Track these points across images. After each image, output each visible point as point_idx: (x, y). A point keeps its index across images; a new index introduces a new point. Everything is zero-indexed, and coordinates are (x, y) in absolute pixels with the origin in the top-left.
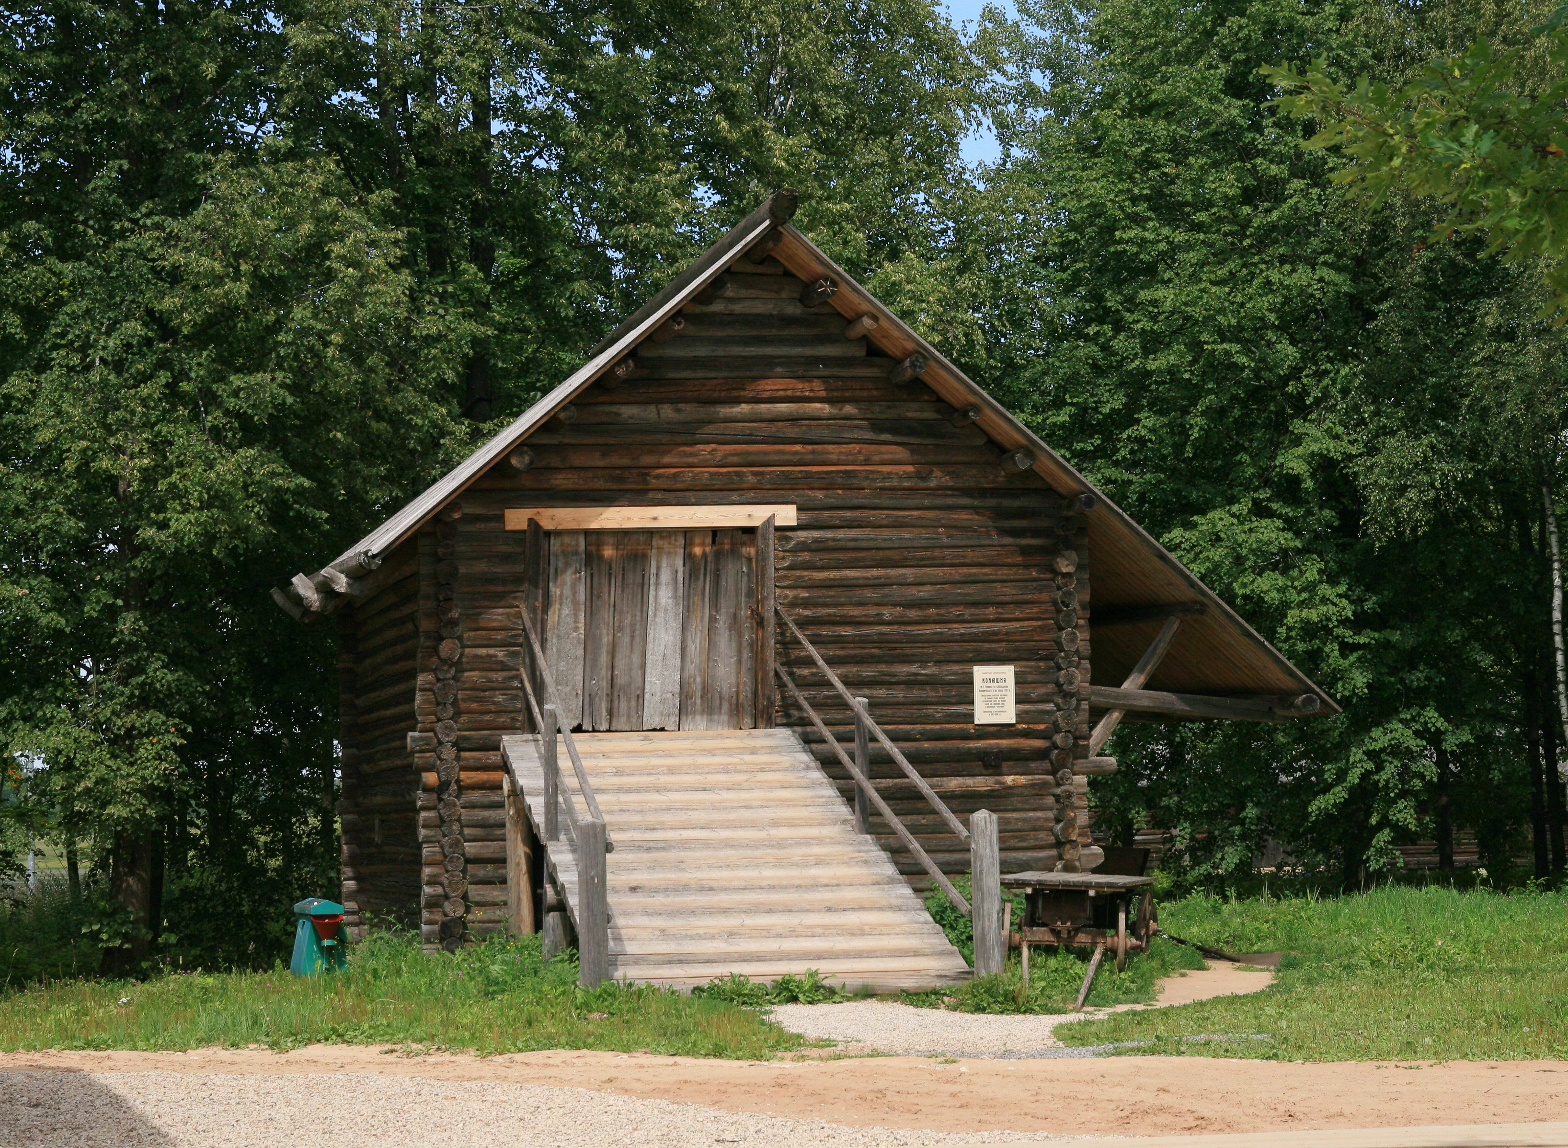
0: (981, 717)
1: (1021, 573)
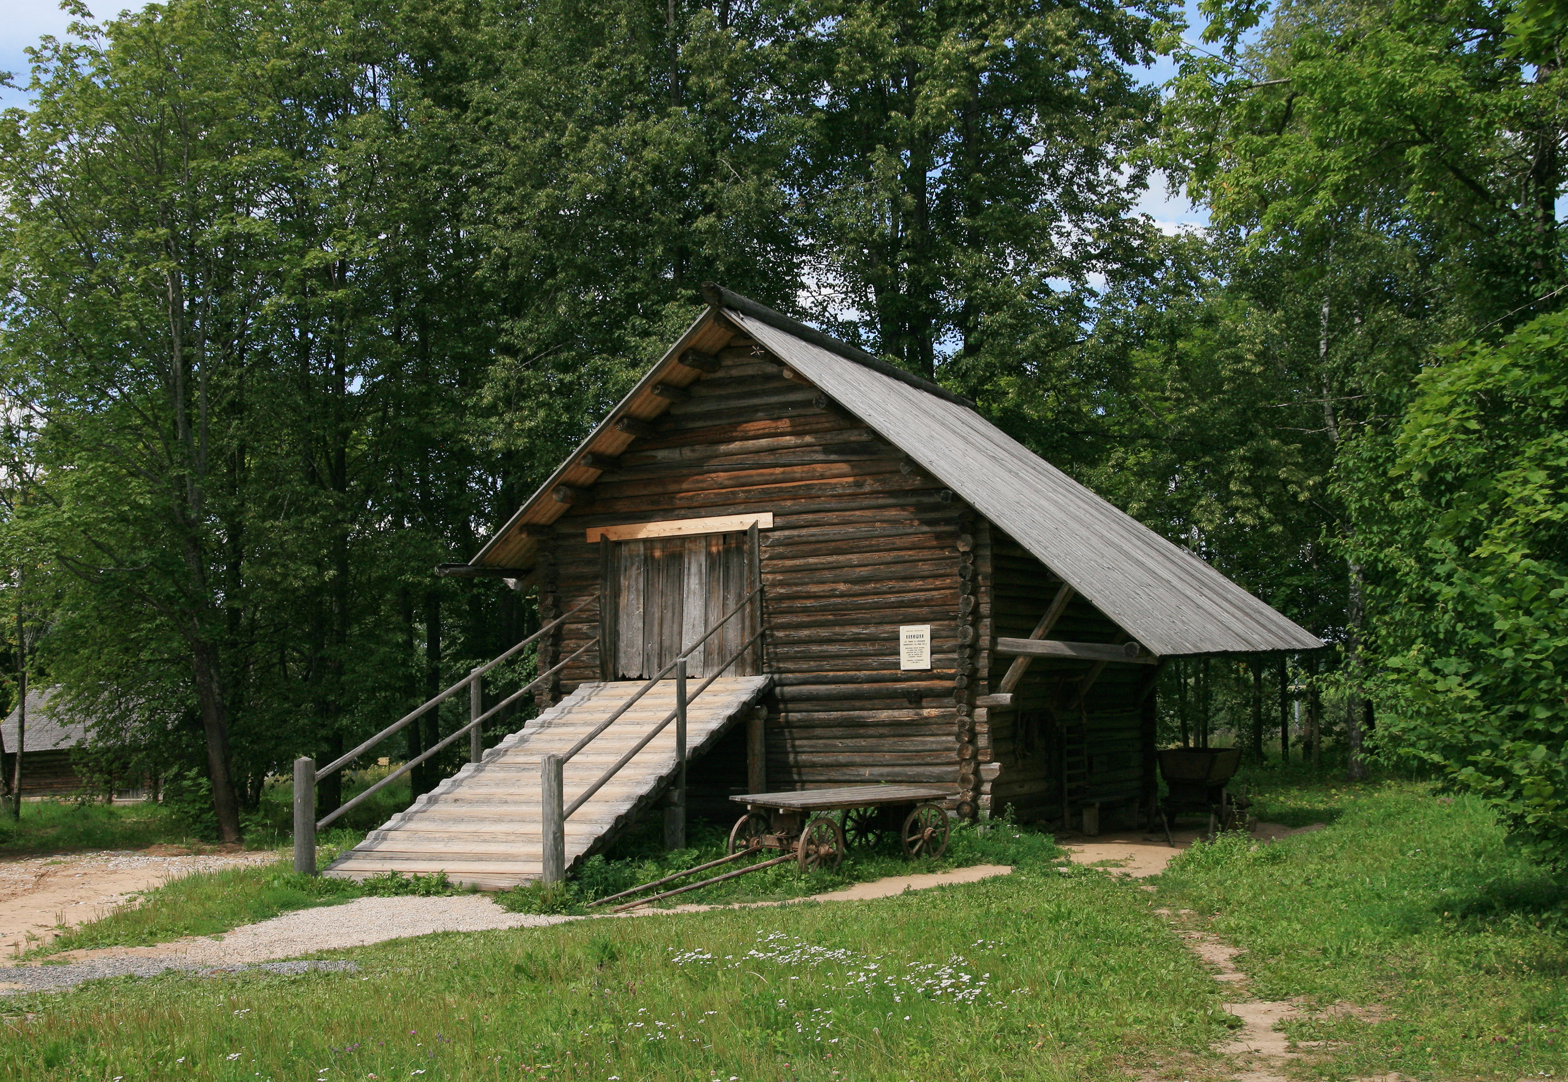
1: (938, 553)
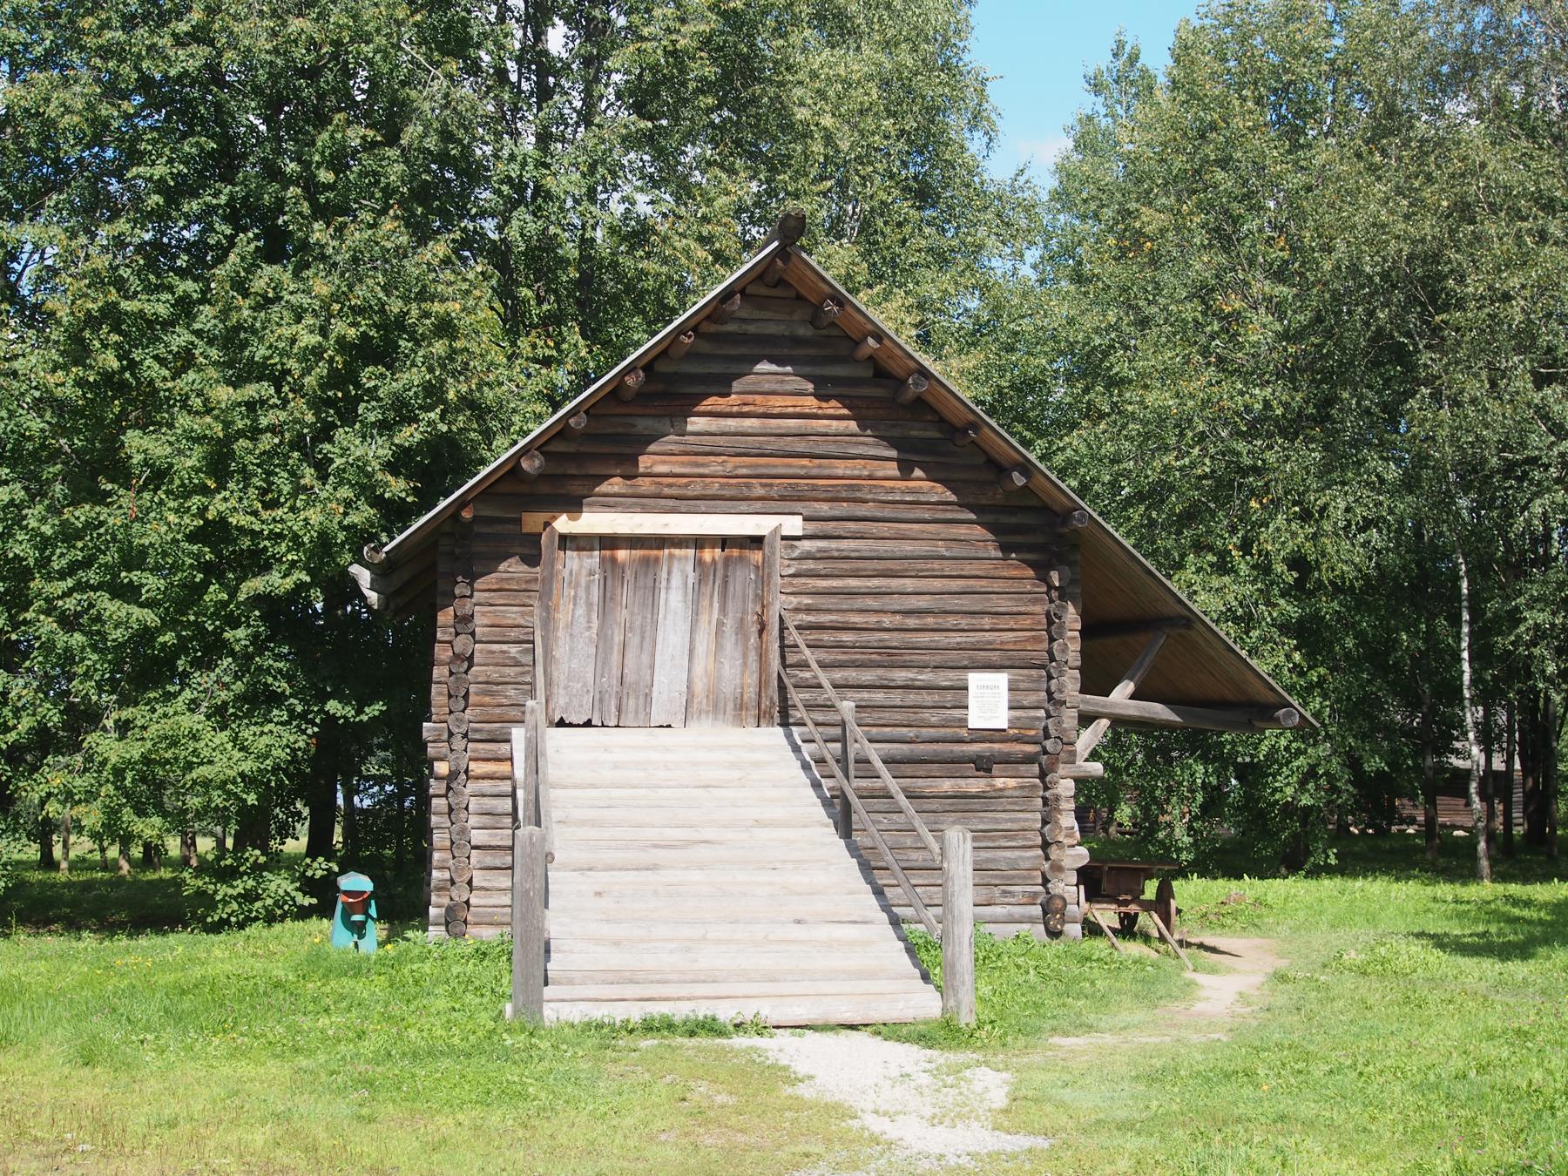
0: (973, 723)
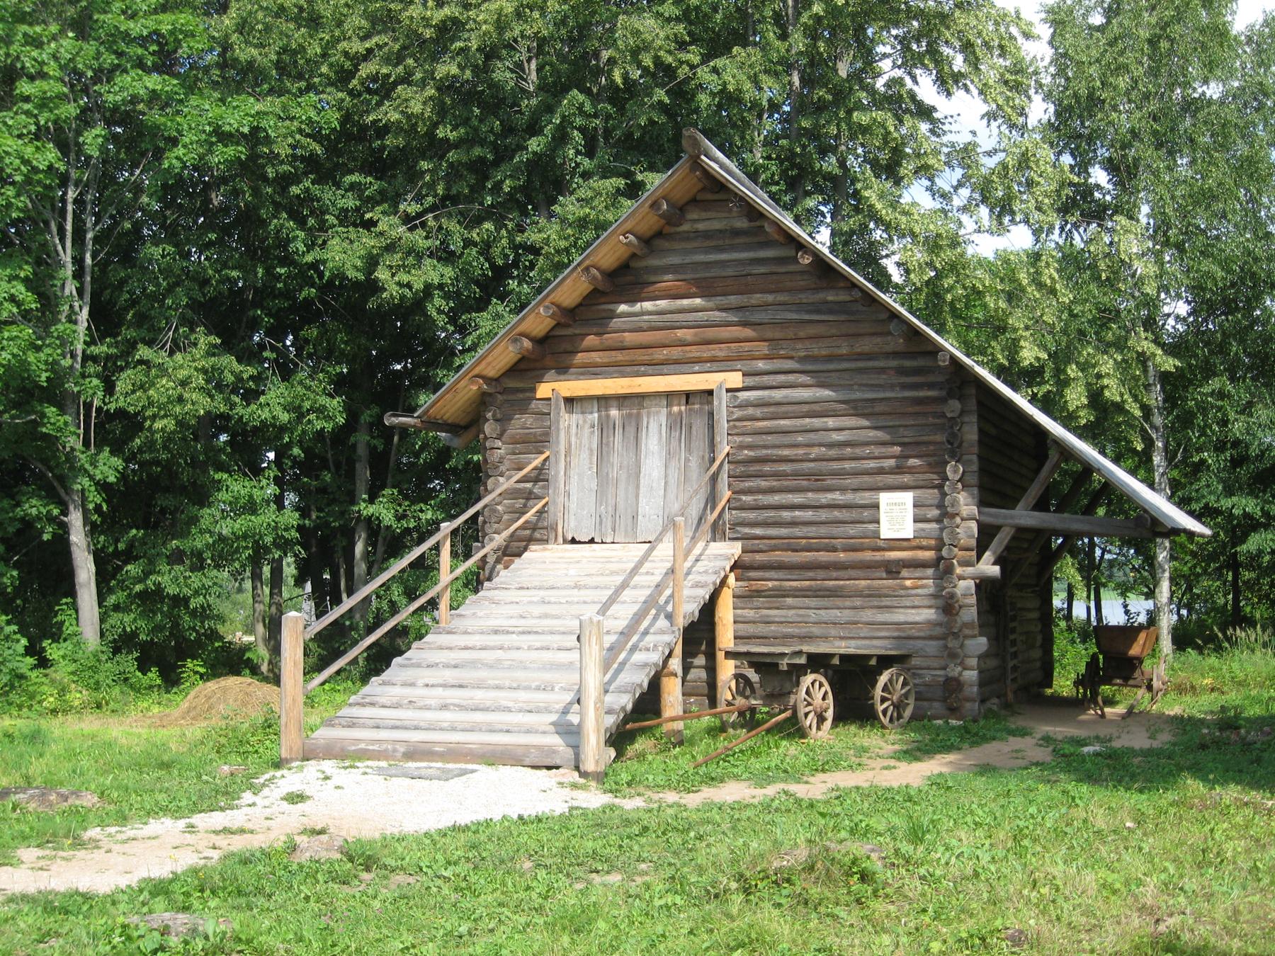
0: (885, 534)
